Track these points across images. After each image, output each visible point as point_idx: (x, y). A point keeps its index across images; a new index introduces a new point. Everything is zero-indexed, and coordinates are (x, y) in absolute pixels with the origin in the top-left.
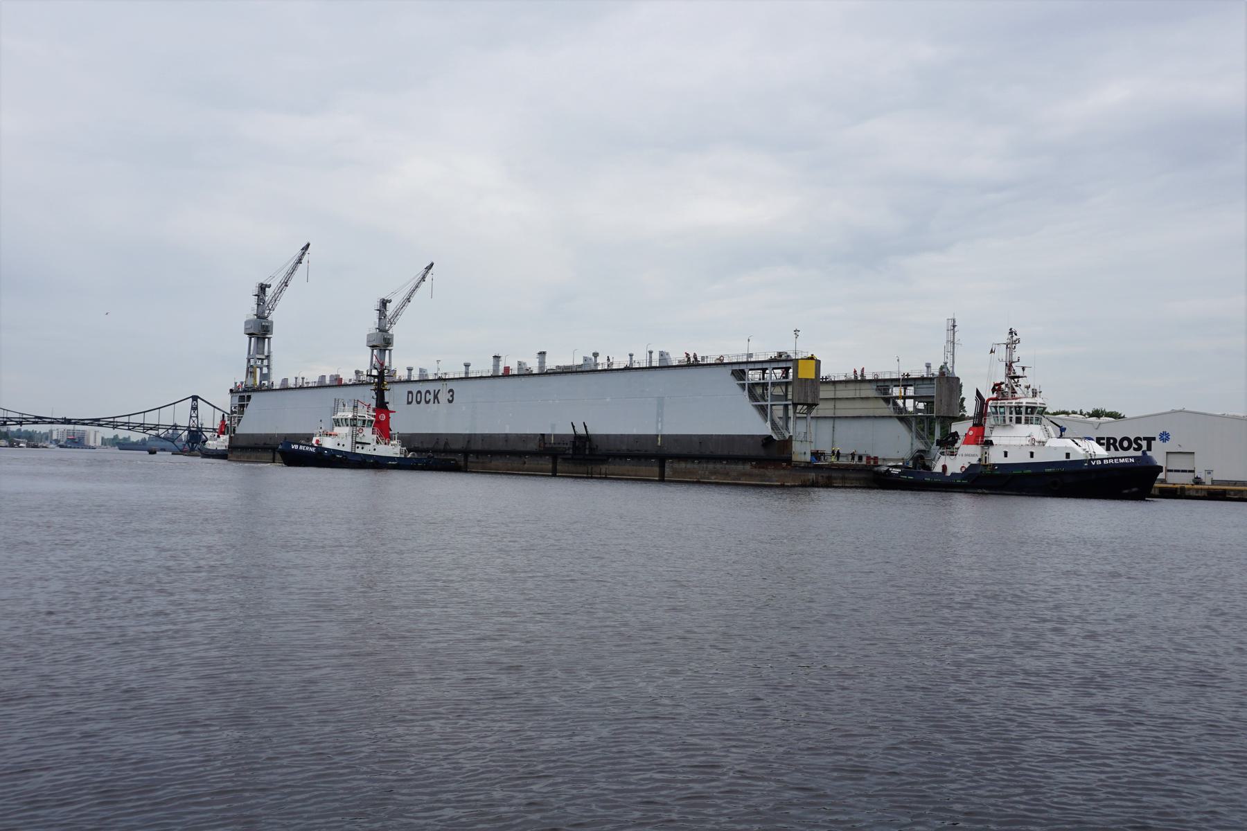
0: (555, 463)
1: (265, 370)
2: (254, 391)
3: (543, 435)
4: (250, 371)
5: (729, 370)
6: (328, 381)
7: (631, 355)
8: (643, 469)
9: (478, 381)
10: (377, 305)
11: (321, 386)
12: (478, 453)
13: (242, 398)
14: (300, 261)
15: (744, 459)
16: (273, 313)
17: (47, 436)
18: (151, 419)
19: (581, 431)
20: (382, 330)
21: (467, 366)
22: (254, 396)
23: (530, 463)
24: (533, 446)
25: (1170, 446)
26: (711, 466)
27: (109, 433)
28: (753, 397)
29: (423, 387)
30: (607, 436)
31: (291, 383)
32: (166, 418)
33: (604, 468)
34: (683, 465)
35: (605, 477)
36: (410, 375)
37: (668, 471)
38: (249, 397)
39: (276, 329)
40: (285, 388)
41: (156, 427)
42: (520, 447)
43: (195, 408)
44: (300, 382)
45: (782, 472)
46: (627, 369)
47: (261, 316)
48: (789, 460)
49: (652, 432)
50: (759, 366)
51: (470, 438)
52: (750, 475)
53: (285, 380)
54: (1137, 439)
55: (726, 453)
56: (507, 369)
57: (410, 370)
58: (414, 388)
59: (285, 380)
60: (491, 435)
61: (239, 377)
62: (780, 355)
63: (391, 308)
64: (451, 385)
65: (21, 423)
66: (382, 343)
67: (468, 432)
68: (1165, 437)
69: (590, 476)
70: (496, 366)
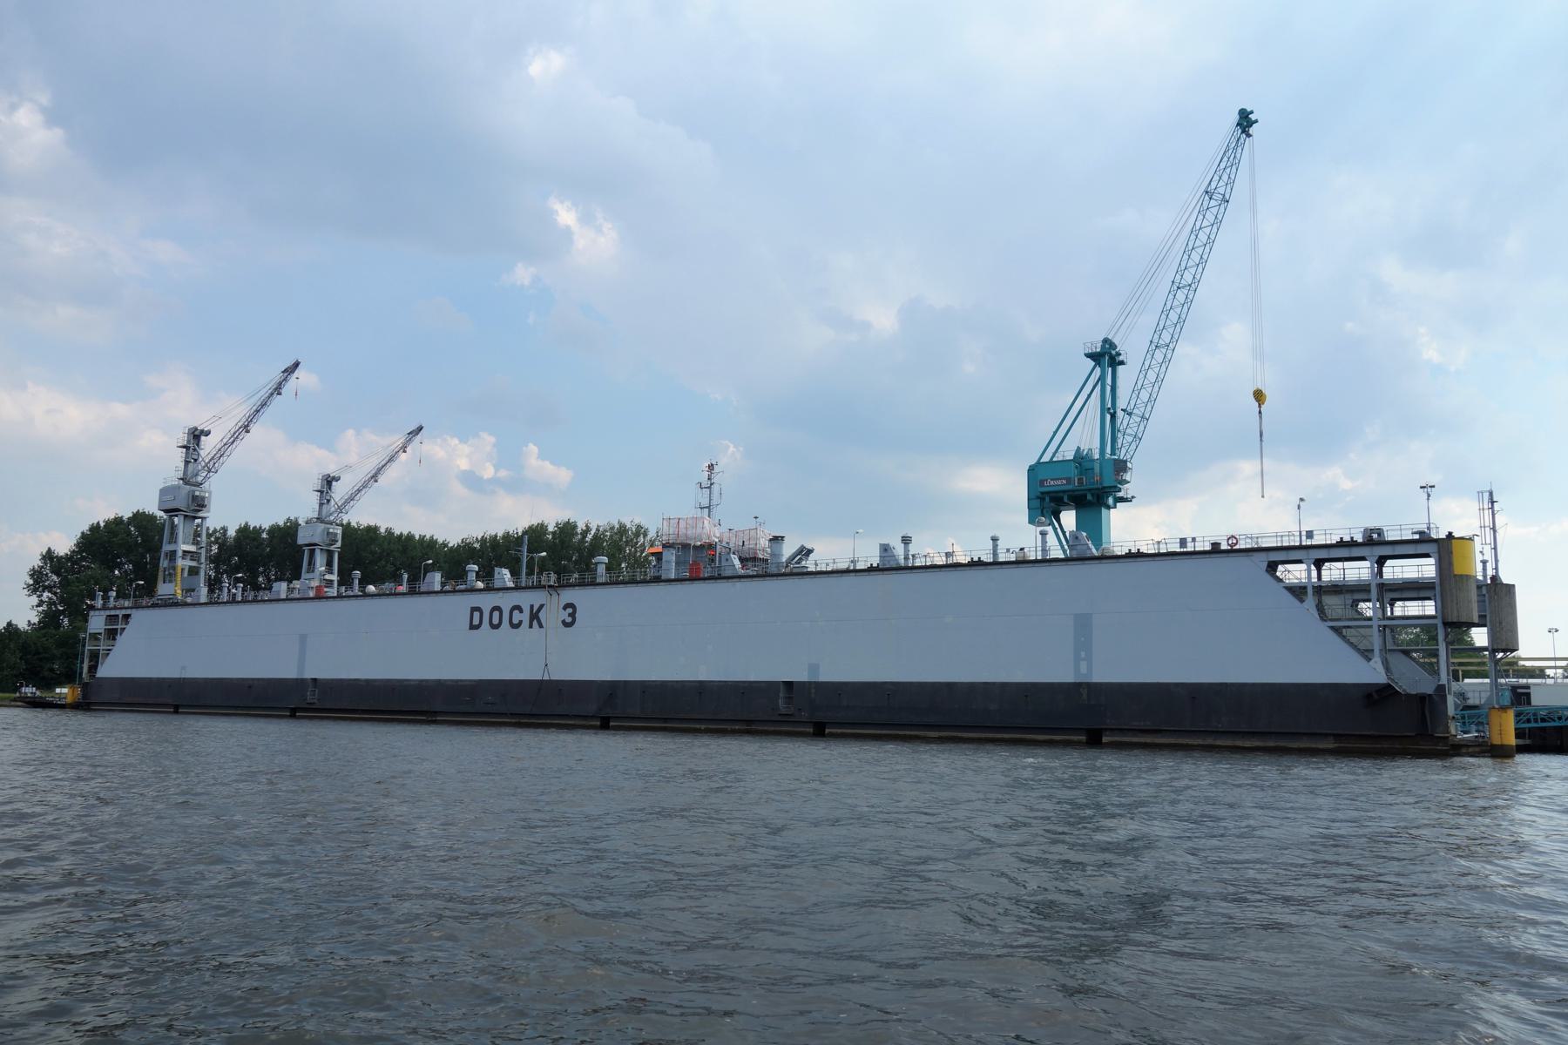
5: (1262, 561)
7: (995, 539)
10: (183, 438)
14: (278, 390)
16: (214, 478)
38: (127, 617)
46: (1017, 563)
60: (663, 686)
62: (1368, 532)
63: (208, 445)
66: (1076, 490)
67: (609, 678)
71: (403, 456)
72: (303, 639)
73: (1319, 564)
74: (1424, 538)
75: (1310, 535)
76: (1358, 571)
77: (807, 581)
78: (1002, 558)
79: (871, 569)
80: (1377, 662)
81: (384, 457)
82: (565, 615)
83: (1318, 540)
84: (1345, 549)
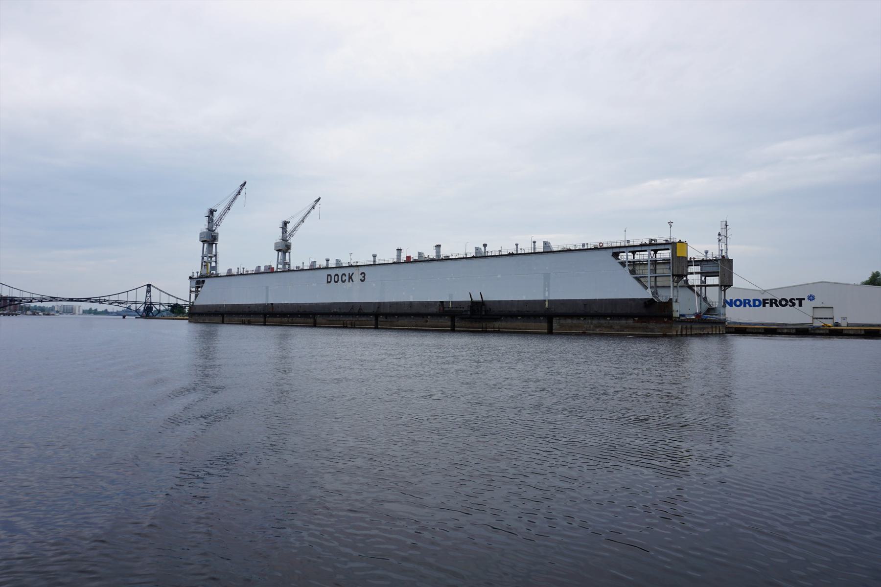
0: (453, 321)
1: (213, 264)
2: (207, 277)
3: (442, 302)
4: (204, 264)
5: (610, 252)
6: (262, 269)
7: (517, 245)
8: (532, 325)
9: (508, 258)
11: (258, 273)
12: (386, 315)
13: (198, 282)
14: (239, 193)
15: (627, 316)
17: (52, 309)
18: (123, 298)
19: (477, 298)
20: (284, 240)
21: (374, 256)
22: (207, 281)
23: (431, 321)
24: (434, 310)
25: (814, 303)
26: (595, 322)
27: (87, 306)
28: (632, 272)
29: (340, 272)
30: (499, 302)
31: (234, 272)
32: (131, 297)
33: (497, 324)
34: (569, 321)
35: (498, 332)
36: (327, 264)
37: (555, 325)
38: (203, 282)
39: (220, 238)
40: (299, 270)
41: (126, 302)
42: (423, 310)
43: (149, 291)
44: (241, 272)
45: (664, 325)
47: (210, 230)
48: (670, 317)
49: (542, 298)
50: (632, 249)
51: (380, 305)
52: (633, 328)
53: (230, 270)
54: (791, 300)
55: (609, 311)
56: (409, 258)
57: (327, 260)
58: (333, 273)
59: (230, 270)
61: (196, 268)
63: (290, 227)
64: (362, 270)
65: (41, 301)
66: (284, 248)
68: (811, 298)
69: (484, 331)
70: (399, 256)
71: (313, 211)
72: (267, 288)
73: (634, 253)
74: (667, 243)
75: (628, 241)
76: (643, 256)
77: (449, 262)
78: (537, 251)
79: (473, 257)
80: (649, 291)
81: (306, 212)
82: (361, 277)
83: (631, 244)
84: (642, 247)
